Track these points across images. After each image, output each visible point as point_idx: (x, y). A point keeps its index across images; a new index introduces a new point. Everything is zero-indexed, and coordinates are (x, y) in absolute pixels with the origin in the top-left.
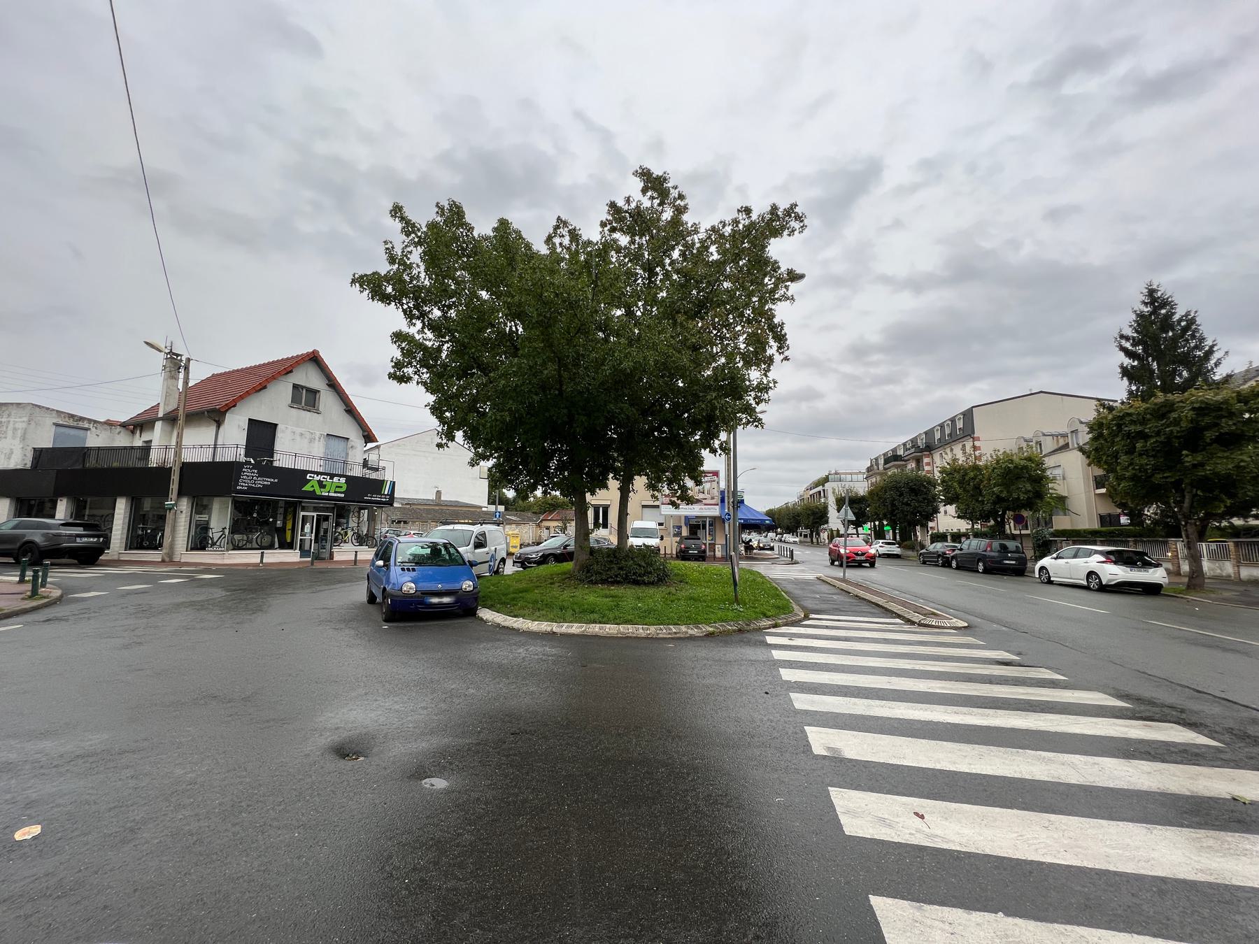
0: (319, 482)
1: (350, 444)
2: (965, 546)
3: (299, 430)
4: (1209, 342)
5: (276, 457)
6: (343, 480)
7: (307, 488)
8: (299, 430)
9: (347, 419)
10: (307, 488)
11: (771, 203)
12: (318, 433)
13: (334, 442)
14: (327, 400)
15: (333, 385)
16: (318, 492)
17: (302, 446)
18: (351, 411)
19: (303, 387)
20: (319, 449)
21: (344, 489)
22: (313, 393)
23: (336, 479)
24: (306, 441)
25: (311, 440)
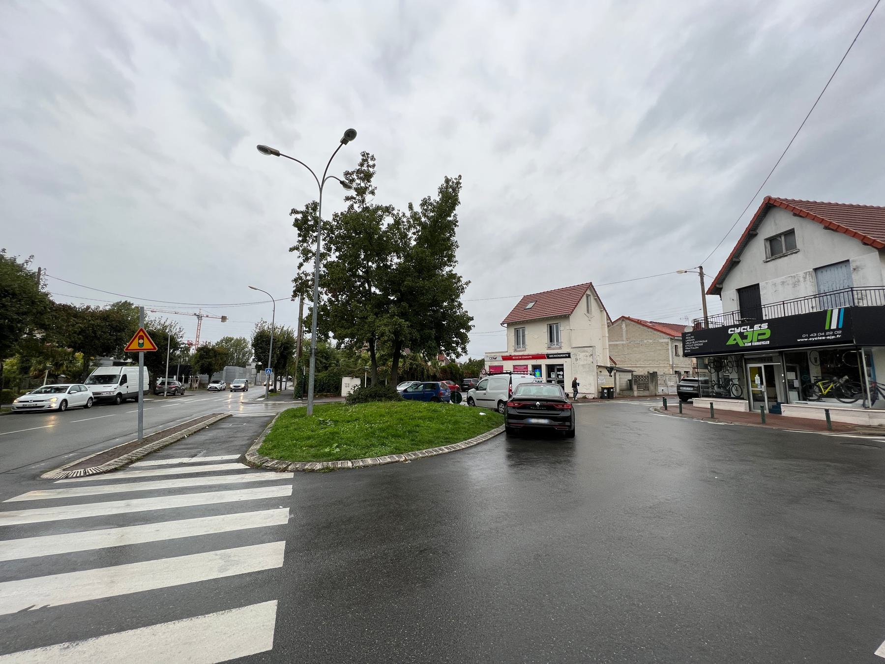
0: (741, 334)
7: (731, 342)
8: (778, 280)
10: (731, 342)
12: (801, 274)
13: (826, 276)
16: (741, 345)
17: (786, 293)
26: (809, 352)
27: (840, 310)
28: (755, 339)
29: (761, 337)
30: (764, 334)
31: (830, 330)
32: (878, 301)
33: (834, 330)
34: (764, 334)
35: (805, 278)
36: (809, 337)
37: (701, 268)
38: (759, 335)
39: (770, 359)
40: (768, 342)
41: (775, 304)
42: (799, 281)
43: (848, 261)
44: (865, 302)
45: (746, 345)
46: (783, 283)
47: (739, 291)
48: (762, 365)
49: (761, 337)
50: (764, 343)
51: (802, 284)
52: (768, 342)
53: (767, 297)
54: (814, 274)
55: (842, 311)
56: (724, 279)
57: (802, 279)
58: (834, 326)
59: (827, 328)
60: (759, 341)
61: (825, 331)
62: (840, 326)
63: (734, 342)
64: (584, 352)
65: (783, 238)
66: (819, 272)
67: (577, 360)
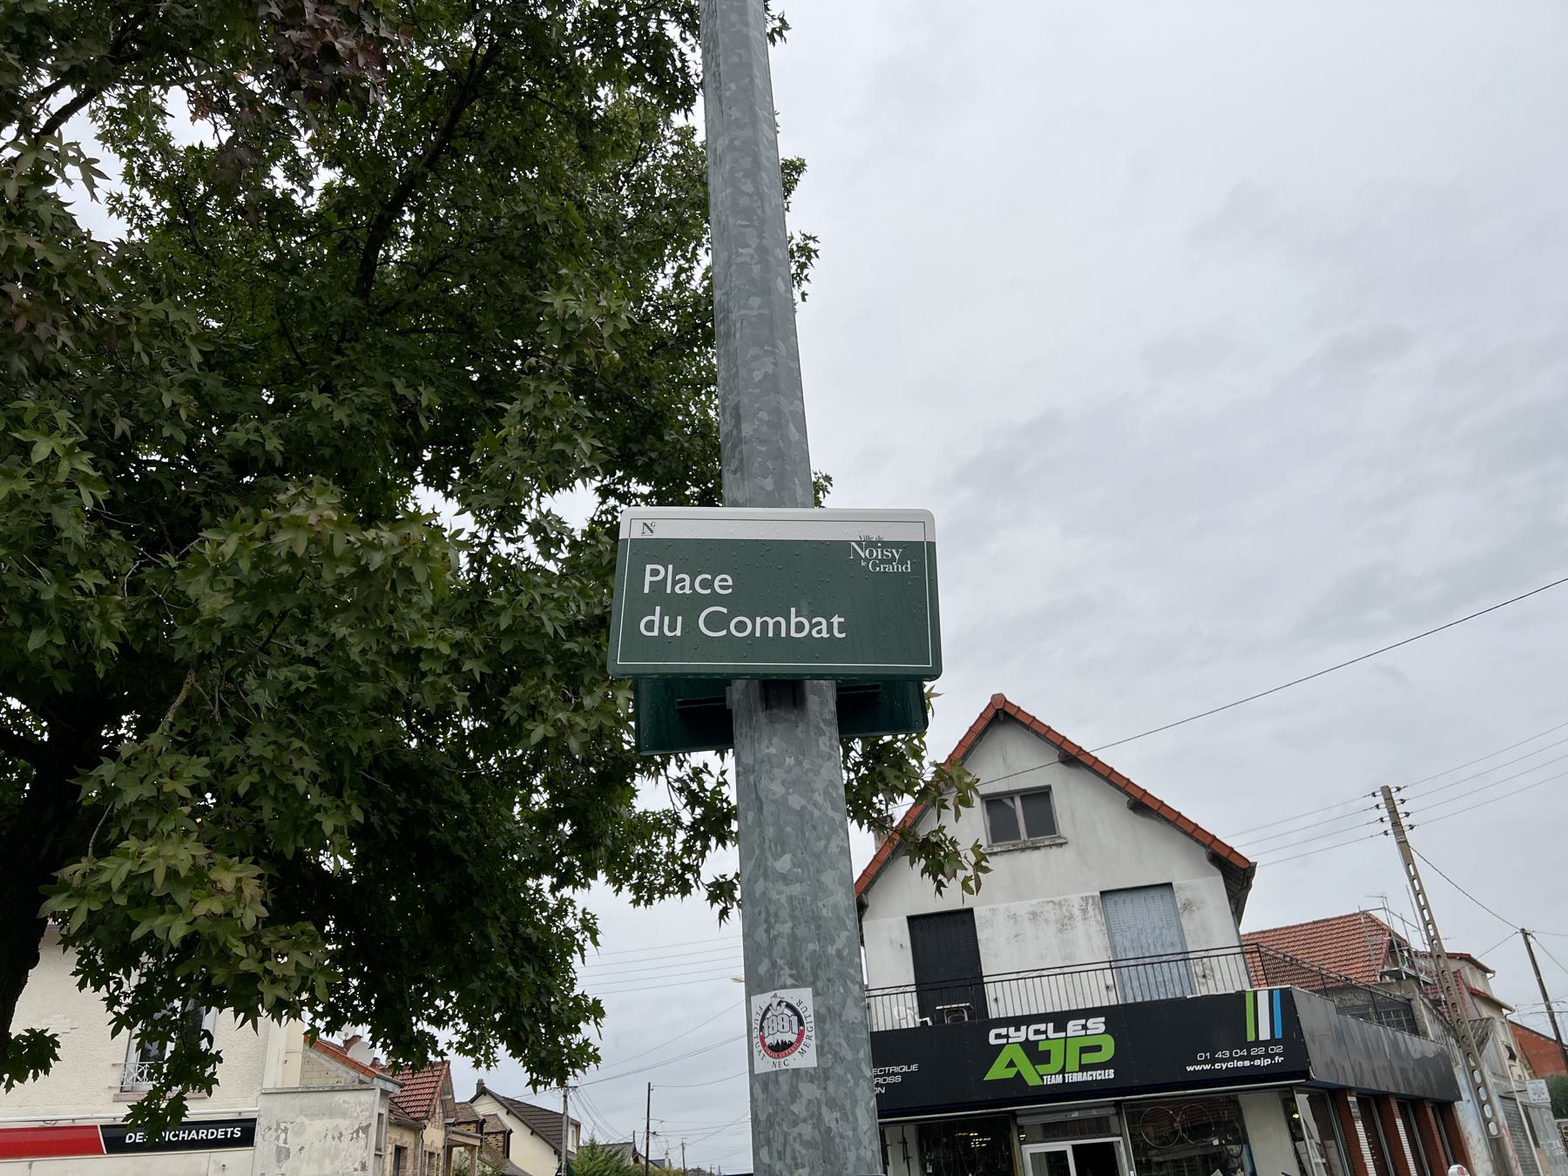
0: (1029, 1047)
1: (1181, 897)
2: (865, 1128)
3: (1023, 907)
4: (865, 827)
5: (990, 991)
6: (1097, 1025)
7: (998, 1071)
8: (1023, 907)
9: (1143, 827)
10: (998, 1071)
11: (924, 519)
12: (1075, 899)
13: (1127, 910)
14: (1074, 802)
15: (1073, 758)
16: (1032, 1079)
17: (1042, 947)
18: (1142, 805)
19: (1011, 795)
20: (1089, 940)
21: (1108, 1052)
22: (1039, 798)
23: (1073, 1027)
24: (1052, 929)
25: (1064, 924)
26: (1242, 1098)
27: (1271, 992)
28: (1073, 1064)
29: (1089, 1058)
30: (1098, 1048)
31: (1258, 1043)
32: (1096, 998)
33: (1265, 1043)
34: (1098, 1048)
35: (1085, 911)
36: (1213, 1061)
37: (1386, 792)
38: (1084, 1050)
39: (1101, 1126)
40: (1111, 1074)
41: (1021, 976)
42: (1071, 917)
43: (1169, 885)
44: (1211, 983)
45: (1048, 1080)
46: (1034, 916)
47: (911, 919)
48: (1066, 1146)
49: (1089, 1058)
50: (1098, 1075)
51: (1079, 923)
52: (1111, 1074)
53: (998, 950)
54: (1098, 899)
55: (1277, 996)
56: (873, 882)
57: (1077, 913)
58: (1265, 1035)
59: (1251, 1037)
60: (1084, 1068)
61: (1250, 1046)
62: (1279, 1035)
63: (1010, 1074)
64: (331, 1112)
65: (1018, 802)
66: (1110, 901)
67: (283, 1154)
